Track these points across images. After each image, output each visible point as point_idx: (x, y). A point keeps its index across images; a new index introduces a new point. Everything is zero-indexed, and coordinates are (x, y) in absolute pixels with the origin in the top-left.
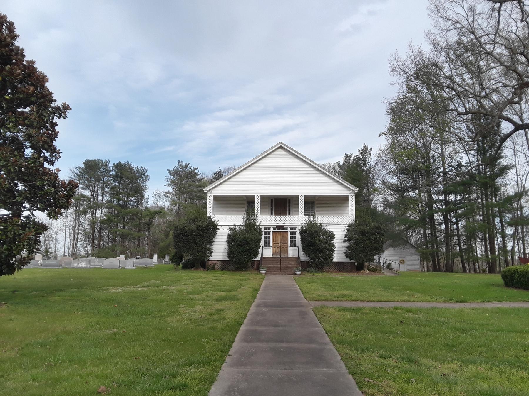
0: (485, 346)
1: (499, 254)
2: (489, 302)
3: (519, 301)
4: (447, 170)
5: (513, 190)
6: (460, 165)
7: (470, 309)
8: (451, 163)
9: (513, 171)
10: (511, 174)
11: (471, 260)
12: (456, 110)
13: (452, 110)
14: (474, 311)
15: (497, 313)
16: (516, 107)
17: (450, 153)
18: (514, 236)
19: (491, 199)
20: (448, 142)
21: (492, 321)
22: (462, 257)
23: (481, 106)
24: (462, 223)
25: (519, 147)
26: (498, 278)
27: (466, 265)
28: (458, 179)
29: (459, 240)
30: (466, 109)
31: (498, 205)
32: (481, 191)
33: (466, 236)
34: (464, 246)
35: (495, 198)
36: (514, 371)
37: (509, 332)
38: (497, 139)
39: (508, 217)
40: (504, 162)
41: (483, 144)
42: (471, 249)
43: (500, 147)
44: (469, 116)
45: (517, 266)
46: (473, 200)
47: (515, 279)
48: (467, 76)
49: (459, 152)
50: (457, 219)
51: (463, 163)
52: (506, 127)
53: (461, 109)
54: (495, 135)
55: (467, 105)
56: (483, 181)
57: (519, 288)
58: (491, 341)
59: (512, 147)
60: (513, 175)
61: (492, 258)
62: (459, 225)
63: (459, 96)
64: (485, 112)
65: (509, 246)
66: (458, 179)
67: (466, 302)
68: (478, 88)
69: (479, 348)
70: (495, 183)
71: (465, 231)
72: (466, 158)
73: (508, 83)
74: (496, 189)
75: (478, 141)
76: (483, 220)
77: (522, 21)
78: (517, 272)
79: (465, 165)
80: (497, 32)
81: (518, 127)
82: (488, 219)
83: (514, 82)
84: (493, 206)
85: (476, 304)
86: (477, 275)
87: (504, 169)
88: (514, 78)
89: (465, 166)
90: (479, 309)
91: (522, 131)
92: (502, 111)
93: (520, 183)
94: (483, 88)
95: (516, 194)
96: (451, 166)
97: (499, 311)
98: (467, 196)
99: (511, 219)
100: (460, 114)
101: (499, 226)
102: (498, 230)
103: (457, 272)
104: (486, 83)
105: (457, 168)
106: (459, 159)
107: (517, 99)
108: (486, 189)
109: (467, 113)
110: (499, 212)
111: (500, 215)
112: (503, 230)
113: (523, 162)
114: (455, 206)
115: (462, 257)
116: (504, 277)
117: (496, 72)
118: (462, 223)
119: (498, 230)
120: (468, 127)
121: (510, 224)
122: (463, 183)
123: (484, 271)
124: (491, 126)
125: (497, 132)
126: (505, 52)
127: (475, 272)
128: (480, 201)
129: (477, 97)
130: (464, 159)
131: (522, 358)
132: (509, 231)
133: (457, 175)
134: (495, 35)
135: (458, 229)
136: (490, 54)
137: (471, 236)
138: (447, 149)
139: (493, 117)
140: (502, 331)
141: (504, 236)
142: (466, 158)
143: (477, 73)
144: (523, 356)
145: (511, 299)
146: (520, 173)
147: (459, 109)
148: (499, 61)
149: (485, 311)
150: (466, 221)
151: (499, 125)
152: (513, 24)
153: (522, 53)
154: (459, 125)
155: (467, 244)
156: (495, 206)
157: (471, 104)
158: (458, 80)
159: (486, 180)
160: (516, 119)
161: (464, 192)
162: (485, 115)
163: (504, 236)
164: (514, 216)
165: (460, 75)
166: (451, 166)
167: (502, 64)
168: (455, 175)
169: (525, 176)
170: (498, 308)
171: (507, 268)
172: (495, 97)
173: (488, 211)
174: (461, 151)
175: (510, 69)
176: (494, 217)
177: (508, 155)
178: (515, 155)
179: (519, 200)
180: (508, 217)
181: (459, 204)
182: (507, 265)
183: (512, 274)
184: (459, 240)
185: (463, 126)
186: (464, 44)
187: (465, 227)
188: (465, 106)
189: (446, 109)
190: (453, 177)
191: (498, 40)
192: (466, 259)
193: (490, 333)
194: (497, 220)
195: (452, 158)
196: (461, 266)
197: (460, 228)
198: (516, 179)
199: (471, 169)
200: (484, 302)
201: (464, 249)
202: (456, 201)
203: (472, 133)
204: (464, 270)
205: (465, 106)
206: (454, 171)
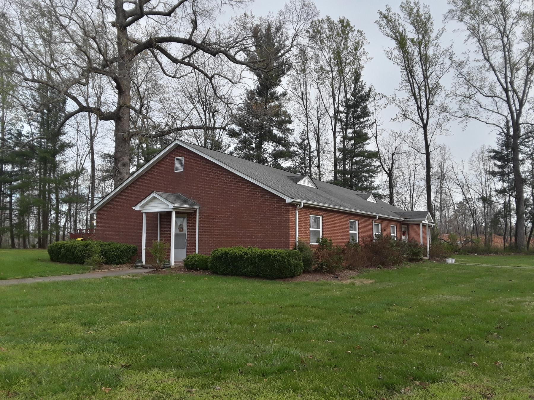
0: (13, 324)
1: (51, 229)
2: (30, 277)
3: (61, 274)
4: (6, 137)
5: (72, 169)
6: (20, 134)
7: (7, 286)
8: (10, 130)
9: (74, 149)
10: (69, 152)
11: (21, 235)
12: (23, 74)
13: (18, 73)
14: (11, 288)
15: (35, 288)
16: (84, 88)
17: (11, 120)
18: (68, 215)
19: (50, 174)
20: (10, 106)
21: (28, 297)
22: (12, 232)
23: (49, 77)
24: (16, 196)
25: (82, 128)
26: (44, 253)
27: (16, 241)
28: (17, 149)
29: (11, 214)
30: (33, 76)
31: (55, 181)
32: (40, 165)
33: (18, 210)
34: (15, 221)
35: (54, 173)
36: (38, 345)
37: (44, 306)
38: (61, 115)
39: (64, 194)
40: (64, 138)
41: (48, 117)
42: (22, 225)
43: (62, 124)
44: (37, 84)
45: (67, 242)
46: (30, 173)
47: (60, 254)
48: (39, 41)
49: (21, 121)
50: (11, 192)
51: (24, 133)
52: (71, 106)
53: (28, 75)
54: (60, 111)
55: (35, 73)
56: (42, 155)
57: (64, 262)
58: (22, 317)
59: (76, 126)
60: (73, 154)
61: (43, 234)
62: (13, 198)
63: (27, 60)
64: (52, 85)
65: (62, 223)
66: (17, 149)
67: (5, 279)
68: (49, 59)
69: (6, 327)
70: (55, 158)
71: (18, 205)
72: (28, 129)
73: (78, 63)
74: (55, 166)
75: (43, 113)
76: (39, 195)
77: (98, 8)
78: (64, 247)
79: (26, 134)
80: (74, 8)
81: (82, 109)
82: (44, 193)
83: (85, 64)
84: (50, 181)
85: (16, 280)
86: (24, 251)
87: (64, 146)
88: (85, 61)
89: (26, 136)
90: (17, 286)
91: (86, 114)
92: (68, 88)
93: (79, 162)
94: (53, 60)
95: (73, 172)
96: (11, 134)
97: (70, 284)
98: (25, 168)
99: (67, 196)
100: (26, 79)
101: (54, 202)
102: (53, 206)
103: (5, 248)
104: (57, 56)
105: (15, 137)
106: (19, 128)
107: (84, 81)
108: (45, 165)
109: (34, 81)
110: (56, 188)
111: (56, 190)
112: (58, 206)
113: (84, 143)
114: (11, 177)
115: (12, 232)
116: (51, 252)
117: (68, 47)
118: (16, 196)
119: (53, 206)
120: (33, 97)
121: (65, 201)
122: (20, 154)
123: (34, 247)
124: (56, 100)
125: (62, 110)
126: (80, 32)
127: (25, 247)
128: (38, 174)
129: (48, 68)
130: (26, 129)
131: (49, 331)
132: (64, 208)
133: (16, 144)
134: (72, 11)
135: (10, 202)
136: (63, 27)
137: (25, 210)
138: (9, 113)
139: (60, 92)
140: (37, 305)
141: (58, 212)
142: (28, 129)
143: (49, 41)
144: (51, 329)
145: (53, 274)
146: (81, 153)
147: (26, 75)
148: (72, 38)
149: (24, 287)
150: (21, 195)
151: (64, 103)
152: (90, 7)
153: (94, 39)
154: (25, 91)
155: (19, 219)
156: (52, 182)
157: (39, 73)
158: (27, 40)
159: (45, 155)
160: (81, 99)
161: (22, 164)
162: (53, 87)
163: (58, 212)
164: (70, 194)
165: (32, 38)
166: (11, 134)
167: (74, 42)
168: (14, 144)
169: (84, 157)
170: (38, 283)
171: (54, 242)
172: (64, 73)
173: (44, 186)
174: (23, 119)
175: (81, 50)
176: (50, 192)
177: (69, 133)
178: (78, 135)
179: (77, 179)
180: (64, 194)
181: (15, 175)
182: (58, 239)
183: (59, 248)
184: (11, 214)
185: (28, 93)
186: (41, 7)
187: (17, 200)
188: (32, 73)
189: (12, 71)
190: (12, 146)
191: (74, 17)
192: (16, 234)
193: (22, 309)
194: (53, 196)
195: (13, 125)
196: (10, 242)
197: (13, 201)
198: (76, 158)
199: (33, 140)
200: (25, 278)
201: (15, 224)
202: (12, 172)
203: (38, 103)
204: (13, 246)
205: (32, 73)
206: (13, 139)
